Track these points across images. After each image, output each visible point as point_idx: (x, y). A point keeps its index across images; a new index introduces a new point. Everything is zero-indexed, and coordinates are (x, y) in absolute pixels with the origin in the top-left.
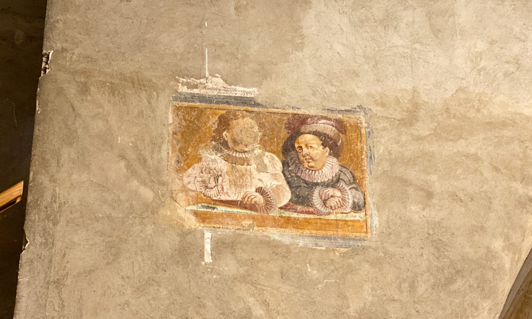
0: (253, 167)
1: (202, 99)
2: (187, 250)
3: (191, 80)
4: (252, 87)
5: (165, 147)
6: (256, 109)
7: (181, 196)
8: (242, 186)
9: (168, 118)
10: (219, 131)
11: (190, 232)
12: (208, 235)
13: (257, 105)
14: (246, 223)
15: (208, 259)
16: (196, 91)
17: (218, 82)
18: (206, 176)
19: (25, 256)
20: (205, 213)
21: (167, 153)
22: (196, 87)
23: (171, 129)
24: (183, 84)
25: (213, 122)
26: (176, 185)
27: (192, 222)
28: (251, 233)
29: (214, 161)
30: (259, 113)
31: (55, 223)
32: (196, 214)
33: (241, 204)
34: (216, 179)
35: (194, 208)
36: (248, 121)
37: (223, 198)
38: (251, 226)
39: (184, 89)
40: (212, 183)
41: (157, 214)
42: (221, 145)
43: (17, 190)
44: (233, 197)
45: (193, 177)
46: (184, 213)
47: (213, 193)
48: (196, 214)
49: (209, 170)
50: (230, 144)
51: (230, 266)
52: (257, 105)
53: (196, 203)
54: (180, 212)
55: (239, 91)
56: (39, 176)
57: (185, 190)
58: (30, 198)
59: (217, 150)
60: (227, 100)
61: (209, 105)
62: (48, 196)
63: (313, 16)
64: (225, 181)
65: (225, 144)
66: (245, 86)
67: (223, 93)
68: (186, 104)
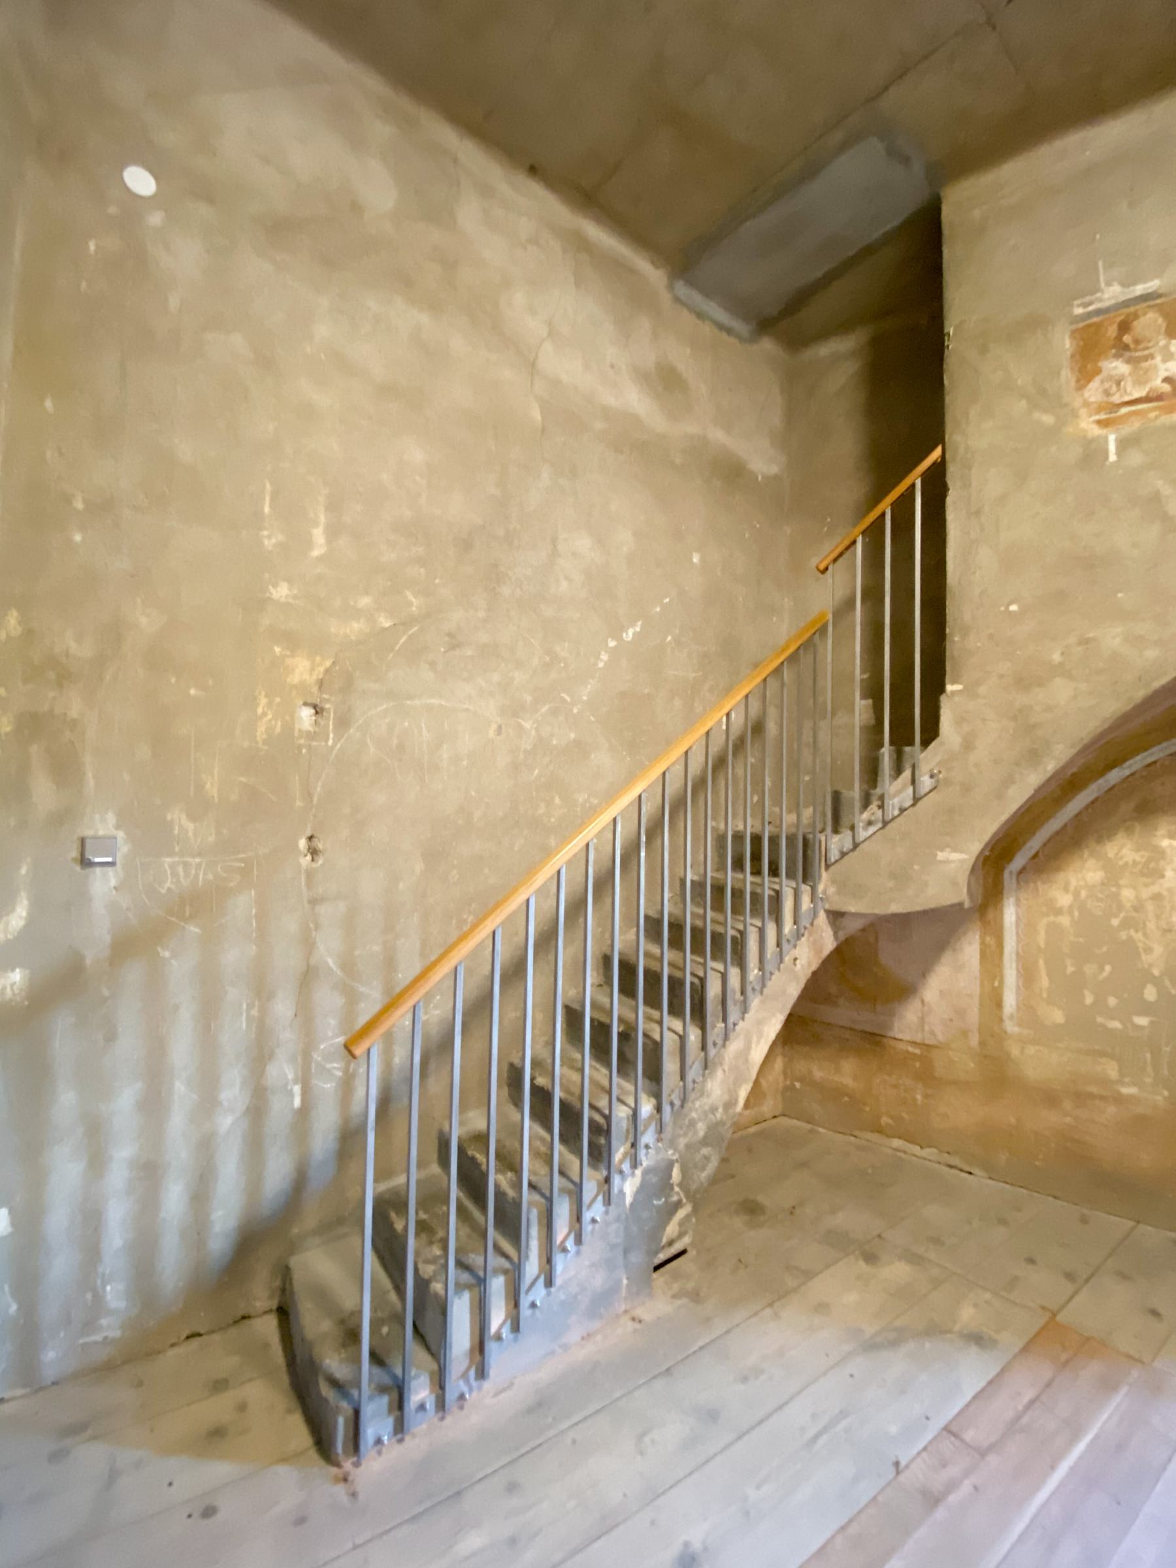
0: (1158, 358)
1: (1098, 312)
2: (1092, 454)
3: (1087, 299)
4: (1152, 280)
5: (1063, 373)
6: (1158, 301)
7: (1083, 412)
8: (1147, 382)
9: (1065, 343)
10: (1119, 338)
11: (1094, 440)
12: (1112, 438)
13: (1160, 296)
14: (1152, 415)
15: (1113, 457)
16: (1091, 308)
17: (1116, 289)
18: (1107, 385)
19: (949, 500)
20: (1108, 419)
21: (1067, 376)
22: (1090, 304)
23: (1069, 353)
24: (1079, 306)
25: (1112, 331)
26: (1078, 402)
27: (1096, 431)
28: (1158, 422)
29: (1115, 368)
30: (1162, 304)
31: (970, 468)
32: (1099, 422)
33: (1146, 399)
34: (1118, 383)
35: (1097, 417)
36: (1151, 315)
37: (1127, 399)
38: (1157, 417)
39: (1079, 311)
40: (1114, 388)
41: (881, 807)
42: (1121, 349)
43: (936, 454)
44: (1137, 395)
45: (1094, 392)
46: (1087, 425)
47: (1117, 399)
48: (1099, 422)
49: (1110, 378)
50: (1132, 346)
51: (1136, 458)
52: (1160, 296)
53: (1098, 412)
54: (1083, 425)
55: (1139, 289)
56: (952, 436)
57: (1086, 404)
58: (948, 456)
59: (1117, 356)
60: (1127, 303)
61: (1107, 316)
62: (961, 450)
63: (587, 1263)
64: (1128, 385)
65: (1126, 347)
66: (1145, 282)
67: (1122, 298)
68: (1081, 325)
